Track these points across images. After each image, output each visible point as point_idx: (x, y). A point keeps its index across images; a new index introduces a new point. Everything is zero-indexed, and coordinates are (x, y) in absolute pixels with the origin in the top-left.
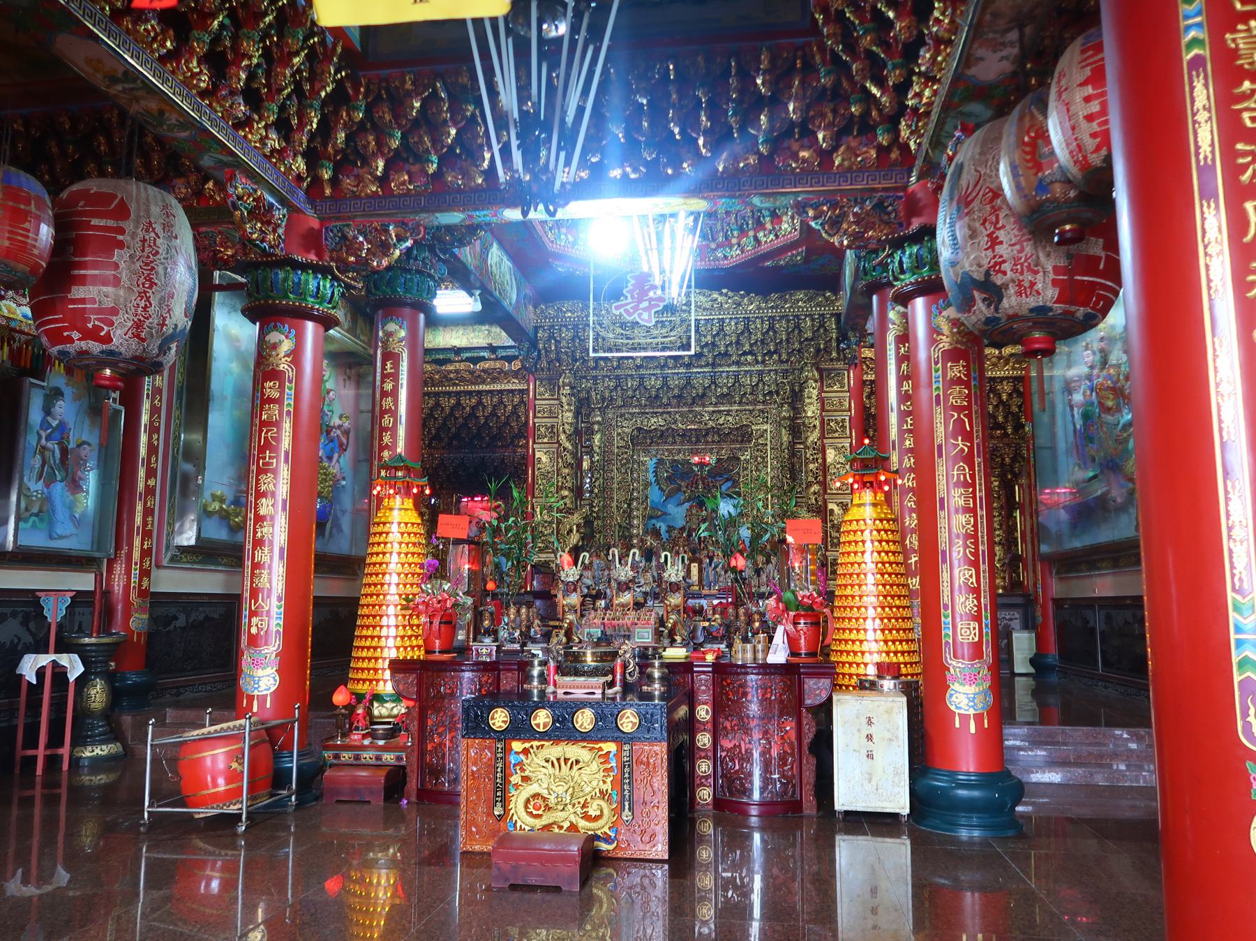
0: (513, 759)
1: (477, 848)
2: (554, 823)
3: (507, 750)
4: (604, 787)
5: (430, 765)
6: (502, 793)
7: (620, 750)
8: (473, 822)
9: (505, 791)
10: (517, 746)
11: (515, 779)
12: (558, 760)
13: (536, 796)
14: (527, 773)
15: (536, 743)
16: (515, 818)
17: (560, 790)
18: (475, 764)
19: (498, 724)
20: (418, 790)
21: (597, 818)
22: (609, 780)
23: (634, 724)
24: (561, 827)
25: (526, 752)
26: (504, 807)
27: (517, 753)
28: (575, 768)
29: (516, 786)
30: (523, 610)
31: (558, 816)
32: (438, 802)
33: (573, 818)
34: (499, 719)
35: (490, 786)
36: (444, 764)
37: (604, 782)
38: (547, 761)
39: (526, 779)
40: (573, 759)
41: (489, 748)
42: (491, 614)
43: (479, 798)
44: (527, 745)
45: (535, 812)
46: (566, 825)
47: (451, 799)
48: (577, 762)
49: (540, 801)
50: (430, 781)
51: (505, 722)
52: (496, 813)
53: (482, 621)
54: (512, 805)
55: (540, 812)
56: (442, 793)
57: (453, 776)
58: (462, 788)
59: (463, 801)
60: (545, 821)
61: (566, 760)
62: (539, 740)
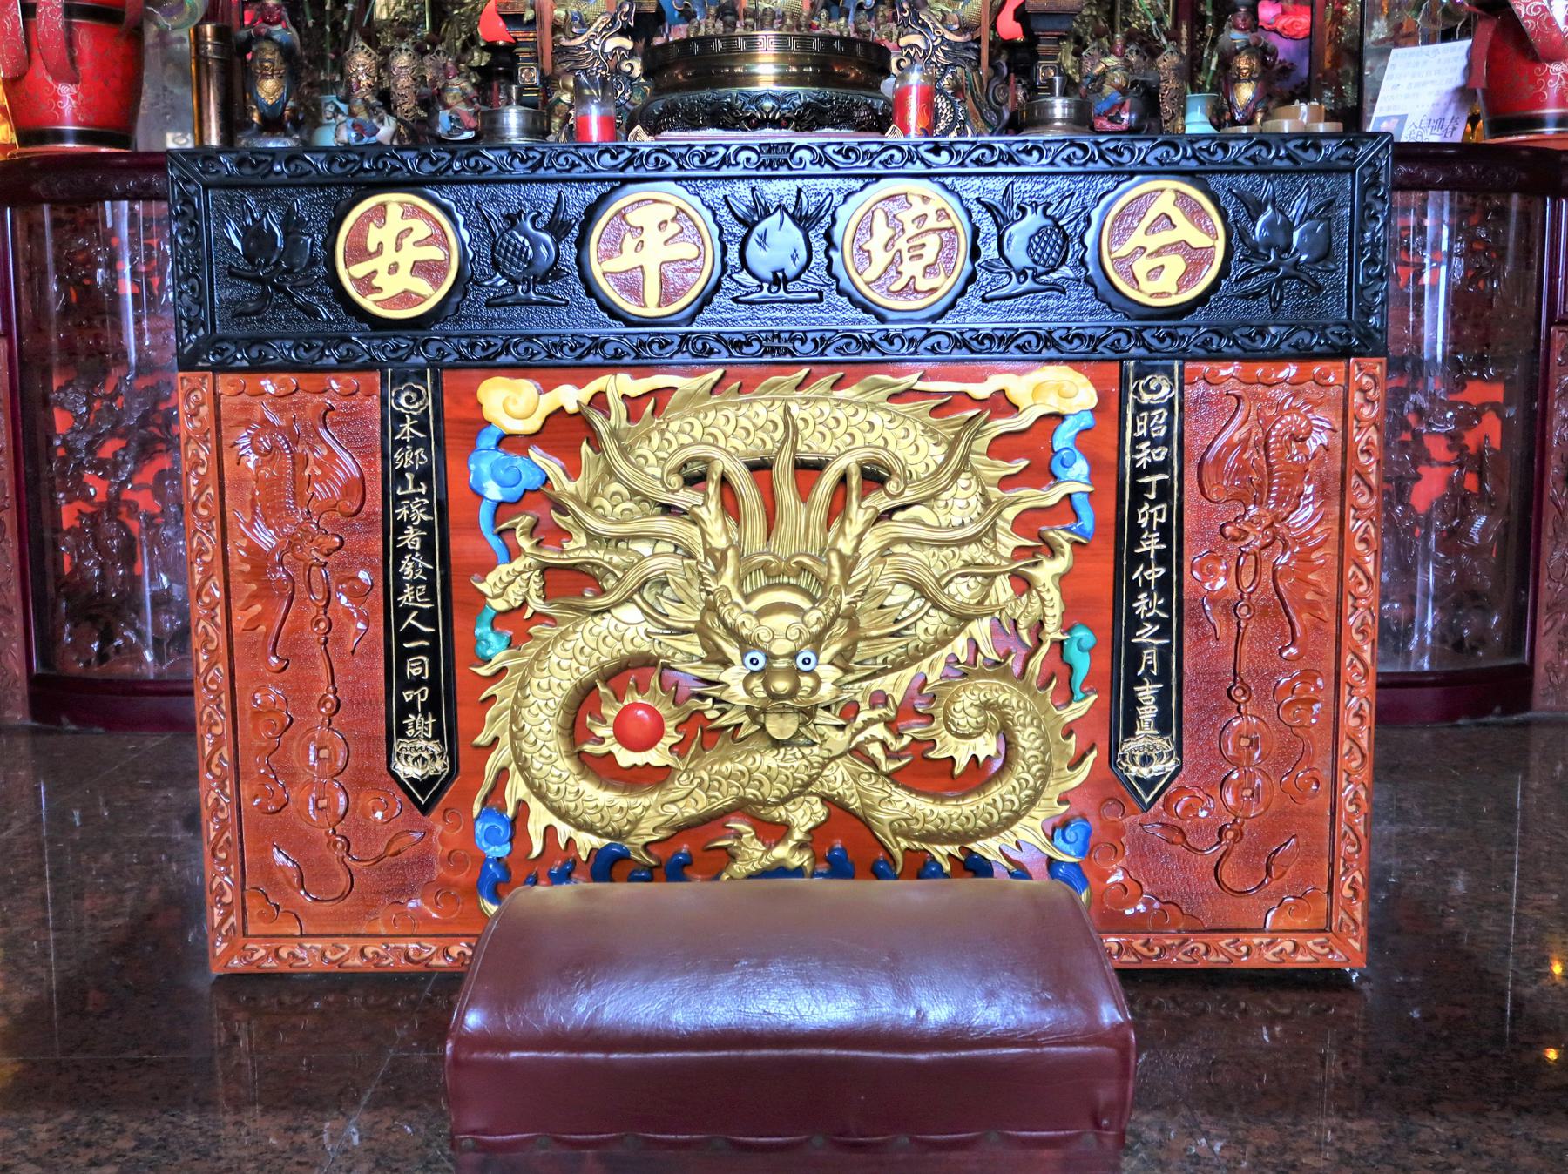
0: (489, 477)
1: (310, 955)
2: (742, 807)
3: (449, 430)
4: (1025, 611)
5: (73, 587)
6: (428, 668)
7: (1115, 406)
8: (278, 821)
9: (444, 653)
10: (511, 402)
11: (507, 583)
12: (760, 468)
13: (629, 670)
14: (577, 549)
15: (618, 385)
16: (516, 789)
17: (781, 633)
18: (272, 511)
19: (391, 286)
20: (33, 680)
21: (979, 775)
22: (1047, 572)
23: (1195, 259)
24: (775, 831)
25: (565, 433)
26: (448, 734)
27: (507, 441)
28: (858, 515)
29: (515, 623)
30: (402, 61)
31: (768, 768)
32: (114, 722)
33: (838, 778)
34: (398, 254)
35: (362, 629)
36: (135, 581)
37: (1024, 584)
38: (694, 480)
39: (571, 585)
40: (848, 462)
41: (344, 422)
42: (287, 52)
43: (299, 693)
44: (569, 397)
45: (626, 758)
46: (805, 816)
47: (164, 707)
48: (874, 477)
49: (647, 699)
50: (79, 647)
51: (423, 269)
52: (408, 770)
53: (250, 79)
54: (494, 726)
55: (656, 756)
56: (136, 688)
57: (169, 623)
58: (207, 669)
59: (209, 712)
60: (685, 800)
61: (809, 469)
62: (641, 369)
